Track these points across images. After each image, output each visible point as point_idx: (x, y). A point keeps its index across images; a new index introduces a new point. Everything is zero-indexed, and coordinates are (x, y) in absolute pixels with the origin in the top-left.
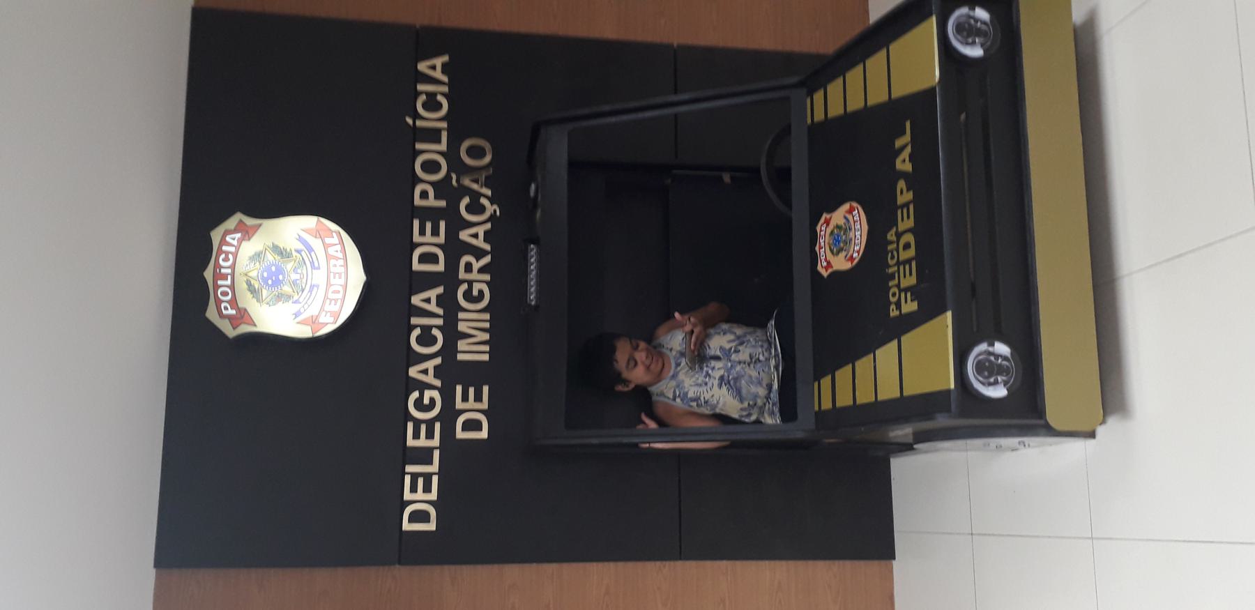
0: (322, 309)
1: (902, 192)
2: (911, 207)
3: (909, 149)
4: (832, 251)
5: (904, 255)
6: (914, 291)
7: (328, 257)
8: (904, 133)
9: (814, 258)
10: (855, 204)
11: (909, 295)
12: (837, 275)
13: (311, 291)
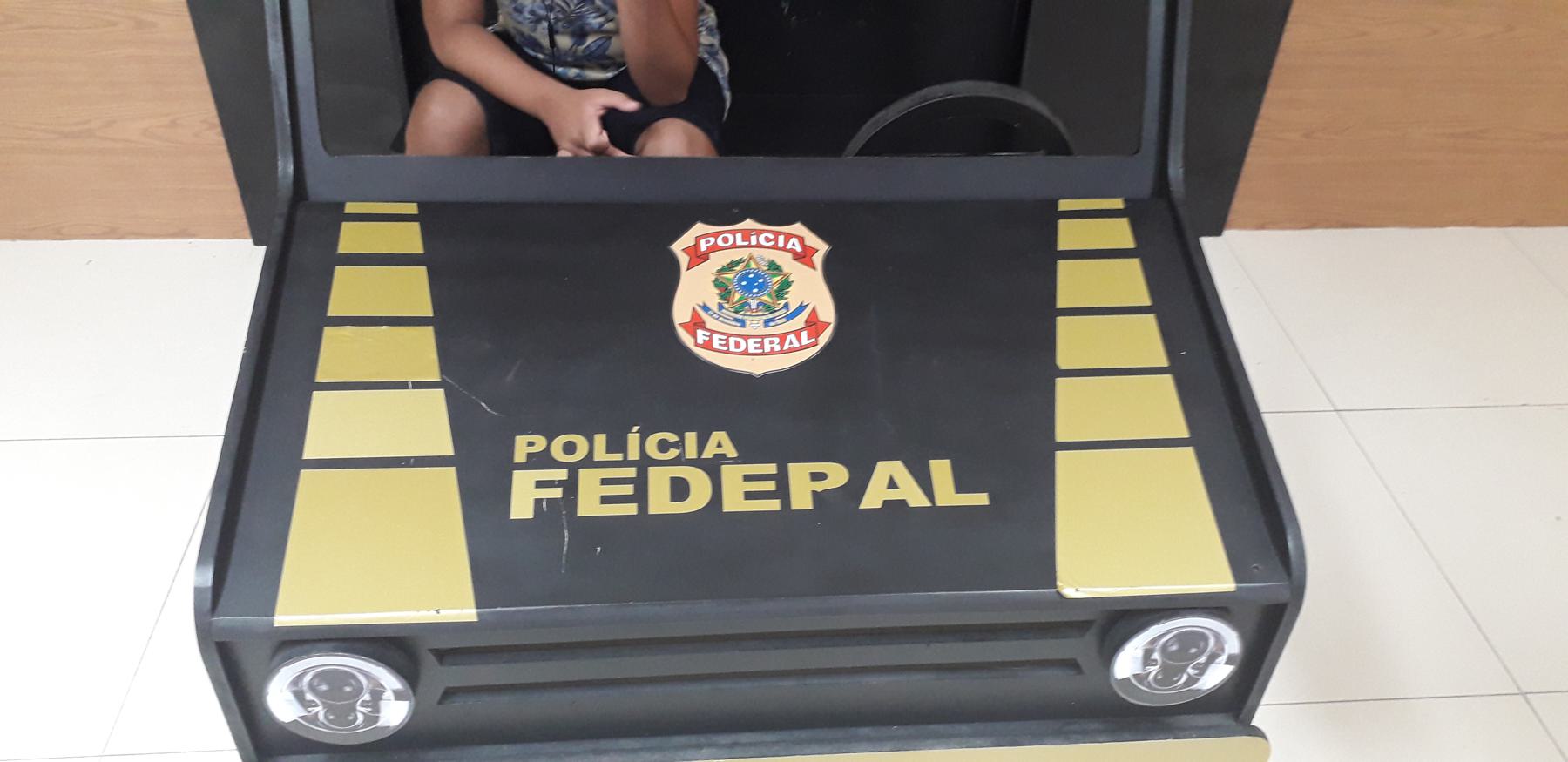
0: (713, 332)
1: (817, 477)
2: (774, 505)
3: (917, 499)
4: (730, 267)
5: (659, 480)
6: (557, 511)
7: (783, 337)
8: (961, 487)
9: (723, 213)
10: (825, 338)
11: (557, 493)
12: (669, 275)
13: (735, 320)
